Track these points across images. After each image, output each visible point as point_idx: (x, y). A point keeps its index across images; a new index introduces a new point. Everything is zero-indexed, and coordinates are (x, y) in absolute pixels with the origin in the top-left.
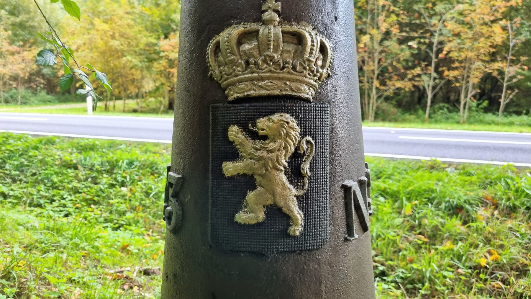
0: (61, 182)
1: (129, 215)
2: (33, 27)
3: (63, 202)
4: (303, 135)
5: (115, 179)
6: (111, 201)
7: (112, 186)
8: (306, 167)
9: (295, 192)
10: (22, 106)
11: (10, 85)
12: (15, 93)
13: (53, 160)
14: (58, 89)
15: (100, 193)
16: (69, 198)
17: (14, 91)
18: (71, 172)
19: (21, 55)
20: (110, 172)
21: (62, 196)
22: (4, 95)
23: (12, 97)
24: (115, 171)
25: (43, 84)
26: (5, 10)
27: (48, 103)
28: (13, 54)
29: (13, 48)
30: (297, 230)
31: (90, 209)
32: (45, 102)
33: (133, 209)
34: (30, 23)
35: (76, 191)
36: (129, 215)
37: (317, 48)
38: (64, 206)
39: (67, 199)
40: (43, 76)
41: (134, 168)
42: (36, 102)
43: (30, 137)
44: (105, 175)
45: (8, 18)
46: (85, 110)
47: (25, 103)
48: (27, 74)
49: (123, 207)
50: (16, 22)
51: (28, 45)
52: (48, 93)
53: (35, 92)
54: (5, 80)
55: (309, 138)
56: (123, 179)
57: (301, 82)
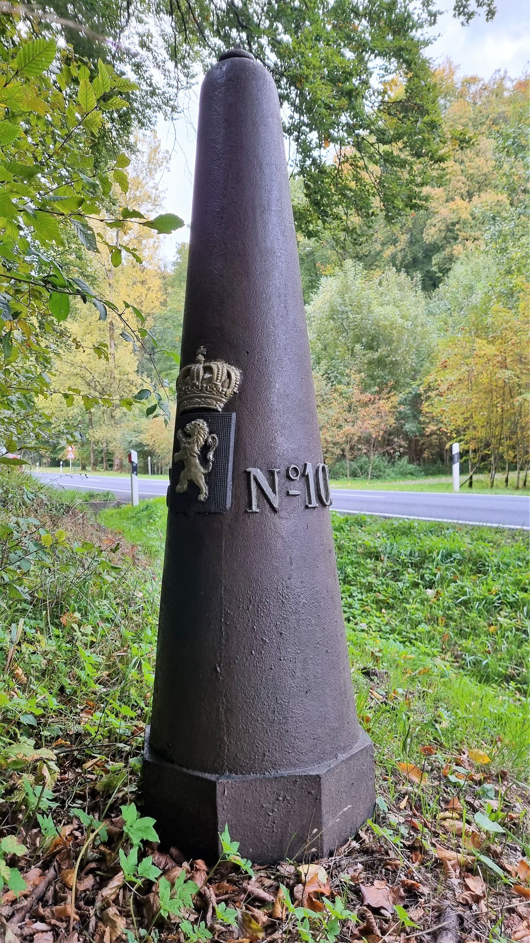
0: (355, 575)
1: (423, 628)
2: (395, 364)
3: (350, 600)
4: (210, 433)
5: (422, 577)
6: (408, 606)
7: (416, 585)
8: (211, 456)
9: (202, 470)
10: (372, 481)
11: (360, 449)
12: (365, 463)
13: (354, 546)
14: (426, 455)
15: (398, 594)
16: (360, 597)
17: (365, 459)
18: (370, 563)
19: (377, 405)
20: (417, 566)
21: (351, 594)
22: (351, 465)
23: (361, 468)
24: (425, 566)
25: (404, 447)
26: (362, 343)
27: (409, 476)
28: (365, 405)
29: (367, 396)
30: (202, 497)
31: (378, 614)
32: (404, 474)
33: (432, 620)
34: (392, 358)
35: (370, 588)
36: (423, 628)
37: (225, 374)
38: (350, 606)
39: (356, 598)
40: (406, 434)
41: (452, 562)
42: (393, 475)
43: (338, 515)
44: (410, 570)
45: (364, 355)
46: (449, 486)
47: (378, 477)
48: (381, 433)
49: (419, 615)
50: (373, 359)
51: (386, 391)
52: (410, 461)
53: (392, 460)
54: (353, 443)
55: (214, 435)
56: (431, 577)
57: (211, 398)
